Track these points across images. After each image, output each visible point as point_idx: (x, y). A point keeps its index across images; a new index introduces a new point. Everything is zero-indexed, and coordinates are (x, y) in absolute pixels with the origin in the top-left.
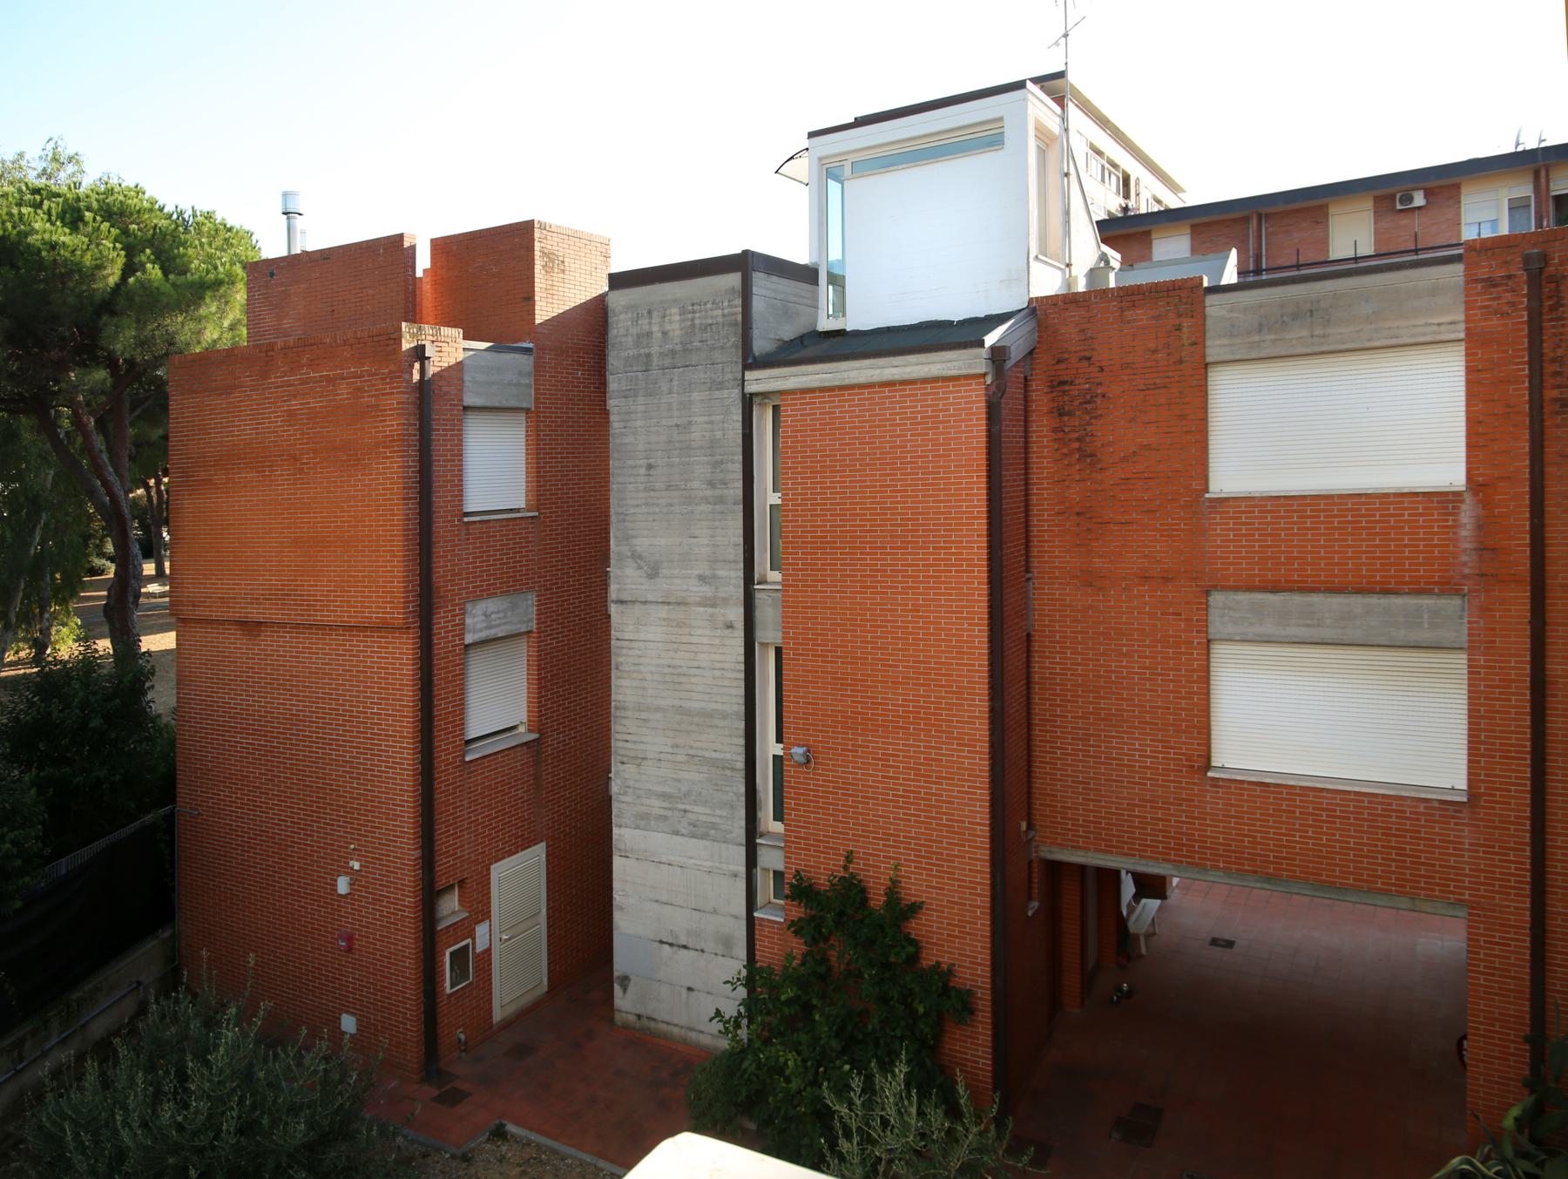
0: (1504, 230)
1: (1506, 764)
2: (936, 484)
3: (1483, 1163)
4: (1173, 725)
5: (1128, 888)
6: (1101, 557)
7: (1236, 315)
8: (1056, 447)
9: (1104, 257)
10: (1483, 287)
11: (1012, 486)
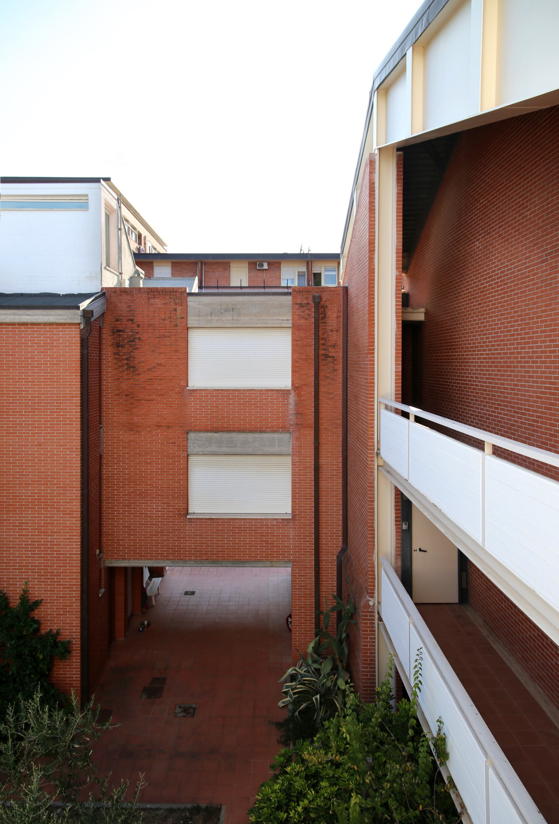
0: (296, 284)
1: (306, 501)
2: (52, 379)
3: (299, 668)
4: (171, 495)
5: (146, 574)
6: (137, 416)
7: (201, 307)
8: (115, 362)
9: (137, 272)
10: (299, 307)
11: (93, 381)
